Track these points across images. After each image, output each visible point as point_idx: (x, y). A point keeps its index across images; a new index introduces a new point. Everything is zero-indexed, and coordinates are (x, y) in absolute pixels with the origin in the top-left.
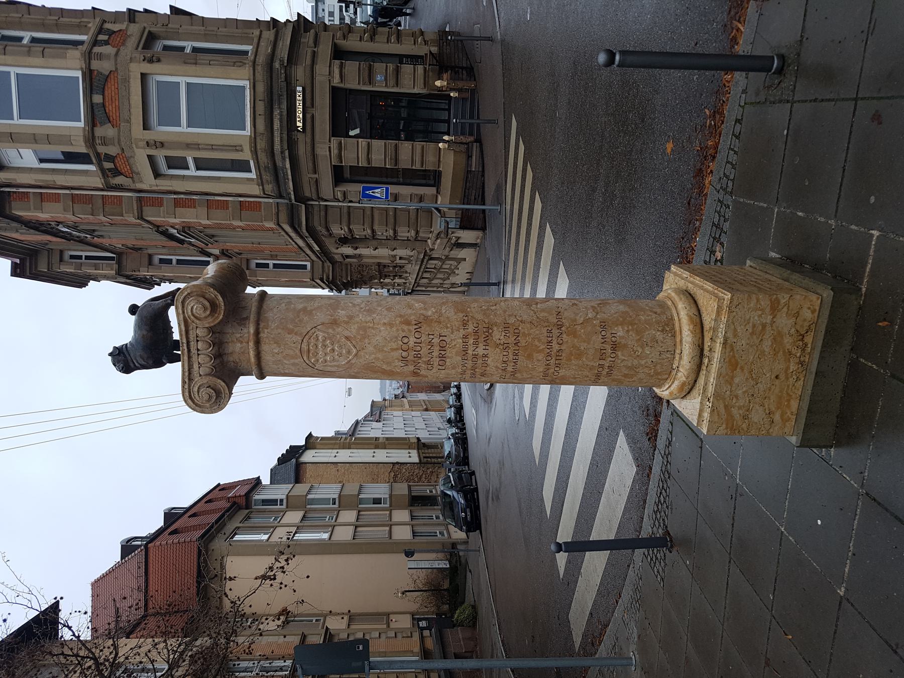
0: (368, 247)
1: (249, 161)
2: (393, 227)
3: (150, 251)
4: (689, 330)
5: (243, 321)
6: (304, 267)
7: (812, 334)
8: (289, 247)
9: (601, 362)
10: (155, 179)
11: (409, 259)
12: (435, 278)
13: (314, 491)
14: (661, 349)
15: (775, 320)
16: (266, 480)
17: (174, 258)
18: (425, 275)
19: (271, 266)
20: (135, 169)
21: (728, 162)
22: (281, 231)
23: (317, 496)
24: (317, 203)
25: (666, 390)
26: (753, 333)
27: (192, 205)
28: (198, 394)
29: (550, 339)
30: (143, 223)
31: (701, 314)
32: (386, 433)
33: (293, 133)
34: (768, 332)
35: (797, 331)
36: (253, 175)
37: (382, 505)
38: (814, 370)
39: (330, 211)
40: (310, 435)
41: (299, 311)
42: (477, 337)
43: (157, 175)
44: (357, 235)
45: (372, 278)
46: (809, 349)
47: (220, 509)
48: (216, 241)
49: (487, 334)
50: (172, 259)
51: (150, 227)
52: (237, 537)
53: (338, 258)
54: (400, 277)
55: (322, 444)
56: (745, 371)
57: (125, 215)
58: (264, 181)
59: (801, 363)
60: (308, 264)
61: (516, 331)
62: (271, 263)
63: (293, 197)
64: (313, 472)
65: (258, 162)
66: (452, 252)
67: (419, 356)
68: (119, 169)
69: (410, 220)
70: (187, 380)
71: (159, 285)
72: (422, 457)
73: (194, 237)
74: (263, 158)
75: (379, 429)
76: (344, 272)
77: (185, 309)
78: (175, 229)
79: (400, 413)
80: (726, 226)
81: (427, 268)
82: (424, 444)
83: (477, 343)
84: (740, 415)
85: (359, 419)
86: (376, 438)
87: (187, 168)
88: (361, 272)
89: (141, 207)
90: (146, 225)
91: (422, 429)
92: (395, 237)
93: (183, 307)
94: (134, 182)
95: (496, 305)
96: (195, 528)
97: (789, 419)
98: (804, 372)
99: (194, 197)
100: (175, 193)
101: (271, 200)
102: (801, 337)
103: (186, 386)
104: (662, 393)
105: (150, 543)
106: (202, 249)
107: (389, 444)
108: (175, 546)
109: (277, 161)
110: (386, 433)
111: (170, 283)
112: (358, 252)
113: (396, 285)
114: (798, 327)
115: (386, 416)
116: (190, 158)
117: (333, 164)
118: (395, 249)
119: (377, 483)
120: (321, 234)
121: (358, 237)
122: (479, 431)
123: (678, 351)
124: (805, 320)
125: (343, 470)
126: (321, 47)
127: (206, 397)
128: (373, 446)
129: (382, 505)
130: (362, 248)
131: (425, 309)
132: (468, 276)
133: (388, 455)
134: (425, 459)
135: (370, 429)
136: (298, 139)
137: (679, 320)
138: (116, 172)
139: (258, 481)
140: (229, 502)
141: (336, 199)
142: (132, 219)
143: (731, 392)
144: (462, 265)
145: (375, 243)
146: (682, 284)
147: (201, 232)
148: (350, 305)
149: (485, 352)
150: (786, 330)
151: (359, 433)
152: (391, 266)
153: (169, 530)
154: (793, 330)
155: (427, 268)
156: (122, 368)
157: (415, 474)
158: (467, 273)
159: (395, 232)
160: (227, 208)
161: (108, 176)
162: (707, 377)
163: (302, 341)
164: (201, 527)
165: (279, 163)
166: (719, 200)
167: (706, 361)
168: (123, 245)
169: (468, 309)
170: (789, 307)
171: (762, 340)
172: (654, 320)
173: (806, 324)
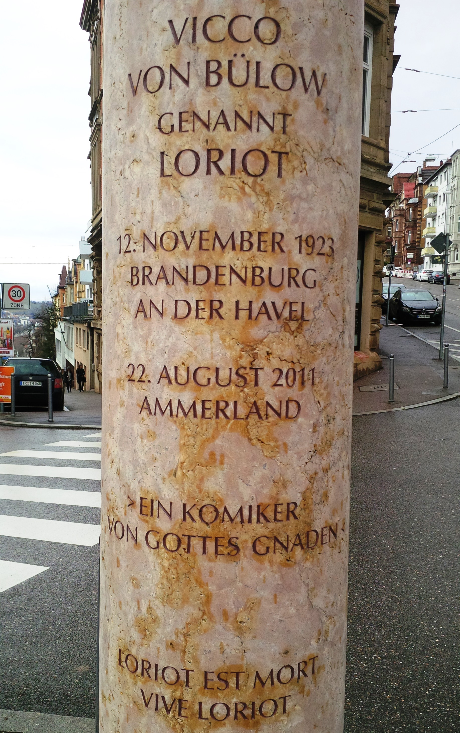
29: (270, 514)
42: (276, 281)
49: (286, 314)
61: (293, 407)
67: (214, 79)
83: (258, 279)
113: (99, 309)
126: (369, 215)
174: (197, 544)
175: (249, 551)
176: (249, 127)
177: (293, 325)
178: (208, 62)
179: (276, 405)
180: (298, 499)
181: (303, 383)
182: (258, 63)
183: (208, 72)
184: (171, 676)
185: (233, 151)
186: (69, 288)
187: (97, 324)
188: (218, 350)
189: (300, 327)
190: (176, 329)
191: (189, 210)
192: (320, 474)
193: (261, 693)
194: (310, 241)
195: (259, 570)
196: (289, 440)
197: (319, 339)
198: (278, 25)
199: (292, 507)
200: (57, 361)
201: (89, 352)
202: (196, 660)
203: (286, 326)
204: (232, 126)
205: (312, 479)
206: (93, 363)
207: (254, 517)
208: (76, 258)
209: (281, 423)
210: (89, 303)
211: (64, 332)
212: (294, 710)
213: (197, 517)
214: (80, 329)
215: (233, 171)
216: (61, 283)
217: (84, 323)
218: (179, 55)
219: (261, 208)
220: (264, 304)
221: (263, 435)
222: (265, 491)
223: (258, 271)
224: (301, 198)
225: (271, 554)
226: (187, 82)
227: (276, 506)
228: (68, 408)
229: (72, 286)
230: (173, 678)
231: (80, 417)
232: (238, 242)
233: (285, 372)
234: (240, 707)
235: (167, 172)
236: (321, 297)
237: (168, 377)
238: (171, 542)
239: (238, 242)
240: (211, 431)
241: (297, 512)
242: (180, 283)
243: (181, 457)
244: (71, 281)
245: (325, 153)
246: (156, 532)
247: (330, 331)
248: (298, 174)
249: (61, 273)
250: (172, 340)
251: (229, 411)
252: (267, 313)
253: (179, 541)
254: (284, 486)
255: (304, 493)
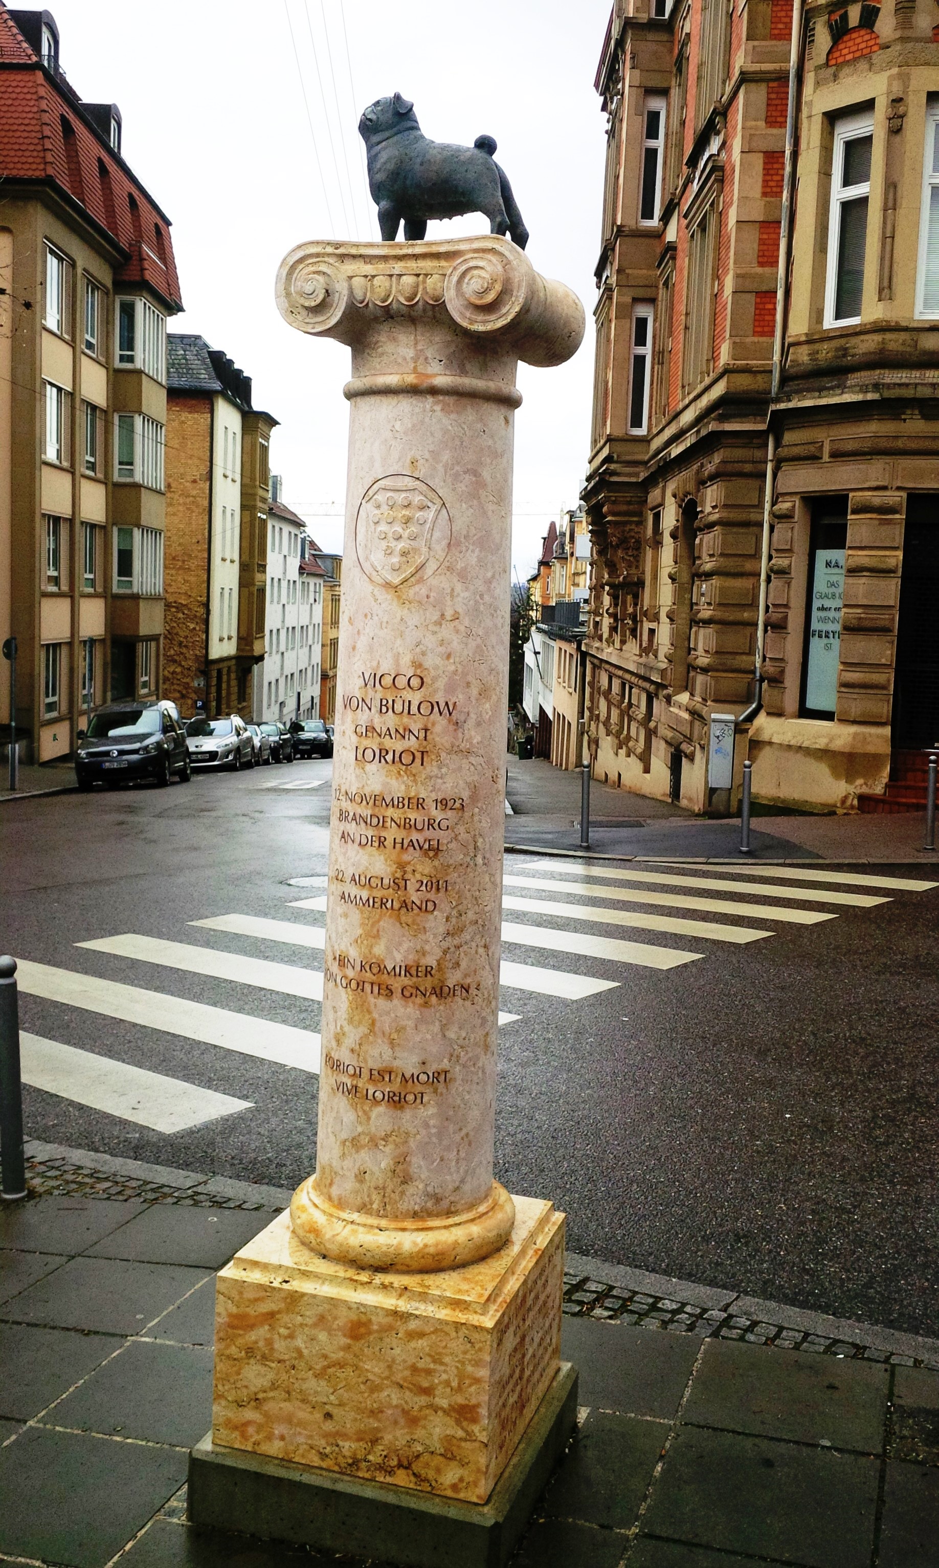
0: (676, 563)
1: (858, 315)
2: (716, 618)
3: (675, 92)
4: (426, 1246)
5: (457, 361)
6: (637, 423)
7: (412, 1486)
8: (679, 391)
9: (365, 1074)
10: (824, 114)
11: (649, 649)
12: (610, 704)
13: (150, 429)
14: (388, 1190)
15: (440, 1413)
16: (175, 325)
17: (659, 144)
18: (616, 683)
19: (640, 350)
20: (846, 70)
21: (781, 1329)
22: (713, 375)
23: (138, 439)
24: (770, 457)
25: (310, 1200)
26: (414, 1369)
27: (769, 190)
28: (314, 273)
29: (414, 972)
30: (733, 82)
31: (458, 1271)
32: (276, 589)
33: (917, 412)
34: (416, 1399)
35: (418, 1457)
36: (829, 322)
37: (115, 577)
38: (340, 1487)
39: (754, 483)
40: (272, 422)
41: (476, 473)
43: (833, 118)
44: (701, 540)
45: (612, 567)
46: (382, 1479)
47: (113, 226)
48: (692, 236)
49: (426, 846)
50: (657, 138)
51: (725, 97)
52: (52, 263)
53: (654, 496)
54: (613, 629)
55: (253, 445)
56: (341, 1354)
57: (751, 43)
58: (817, 346)
59: (355, 1463)
60: (642, 431)
61: (430, 905)
62: (647, 350)
63: (782, 406)
64: (191, 426)
65: (857, 334)
66: (663, 745)
67: (384, 709)
68: (846, 38)
69: (730, 657)
70: (341, 251)
71: (604, 108)
72: (221, 665)
73: (701, 189)
74: (867, 345)
75: (285, 573)
76: (624, 508)
77: (481, 255)
78: (719, 151)
79: (318, 618)
80: (652, 1324)
81: (631, 688)
82: (249, 671)
83: (407, 826)
84: (256, 1342)
85: (306, 529)
86: (264, 566)
87: (846, 183)
88: (624, 545)
89: (767, 81)
90: (728, 89)
91: (282, 666)
92: (695, 622)
93: (484, 251)
94: (818, 68)
95: (485, 864)
96: (75, 172)
97: (244, 1437)
98: (336, 1468)
99: (785, 195)
100: (795, 155)
101: (776, 357)
102: (405, 1463)
103: (330, 250)
104: (305, 1192)
105: (44, 74)
106: (678, 204)
107: (251, 594)
108: (38, 128)
109: (857, 375)
110: (276, 589)
111: (607, 132)
112: (667, 540)
113: (598, 619)
114: (426, 1457)
115: (312, 588)
116: (868, 190)
117: (851, 495)
118: (672, 620)
119: (165, 567)
120: (704, 461)
121: (697, 541)
122: (272, 796)
123: (383, 1223)
124: (438, 1471)
125: (194, 493)
127: (308, 288)
128: (246, 558)
129: (115, 577)
130: (675, 550)
131: (479, 724)
132: (613, 776)
133: (227, 592)
134: (214, 674)
135: (285, 552)
136: (905, 420)
137: (446, 1227)
138: (839, 32)
139: (172, 306)
140: (130, 244)
141: (777, 498)
142: (740, 61)
143: (301, 1325)
144: (635, 765)
145: (685, 577)
146: (519, 1236)
147: (712, 205)
148: (489, 574)
149: (389, 843)
150: (420, 1433)
151: (277, 529)
152: (635, 611)
153: (71, 117)
154: (420, 1448)
155: (631, 688)
156: (370, 120)
157: (184, 650)
158: (620, 775)
159: (707, 622)
160: (761, 264)
161: (830, 13)
162: (332, 1279)
163: (418, 479)
164: (76, 185)
165: (854, 379)
166: (705, 1311)
167: (364, 1277)
168: (688, 35)
169: (477, 810)
170: (466, 1440)
171: (401, 1387)
172: (448, 1177)
173: (431, 1474)
174: (368, 987)
175: (399, 995)
176: (404, 737)
177: (431, 854)
178: (381, 700)
179: (418, 903)
180: (434, 964)
181: (438, 889)
182: (410, 702)
183: (381, 705)
184: (351, 1070)
185: (394, 751)
186: (558, 565)
187: (592, 647)
188: (383, 867)
189: (436, 855)
190: (360, 851)
191: (369, 782)
192: (452, 949)
193: (405, 1087)
194: (444, 802)
195: (406, 1007)
196: (427, 926)
197: (451, 862)
198: (422, 679)
199: (429, 969)
200: (524, 705)
201: (576, 696)
202: (365, 1061)
203: (426, 853)
204: (393, 736)
205: (445, 952)
206: (583, 718)
207: (403, 973)
208: (574, 509)
209: (422, 914)
210: (582, 605)
211: (539, 653)
212: (429, 1103)
213: (368, 969)
214: (565, 651)
215: (393, 762)
216: (544, 556)
217: (570, 641)
218: (366, 692)
219: (410, 784)
220: (411, 841)
221: (410, 921)
222: (411, 957)
223: (408, 821)
224: (437, 777)
225: (413, 997)
226: (370, 709)
227: (418, 967)
228: (513, 809)
229: (563, 561)
230: (352, 1072)
231: (522, 829)
232: (396, 803)
233: (425, 882)
234: (391, 1094)
235: (359, 758)
236: (453, 835)
237: (355, 880)
238: (354, 984)
239: (396, 803)
240: (377, 916)
241: (433, 972)
242: (363, 824)
243: (360, 931)
244: (563, 552)
245: (455, 749)
246: (345, 977)
247: (462, 856)
248: (434, 763)
249: (546, 535)
250: (358, 857)
251: (389, 905)
252: (413, 845)
253: (358, 984)
254: (424, 955)
255: (438, 961)
